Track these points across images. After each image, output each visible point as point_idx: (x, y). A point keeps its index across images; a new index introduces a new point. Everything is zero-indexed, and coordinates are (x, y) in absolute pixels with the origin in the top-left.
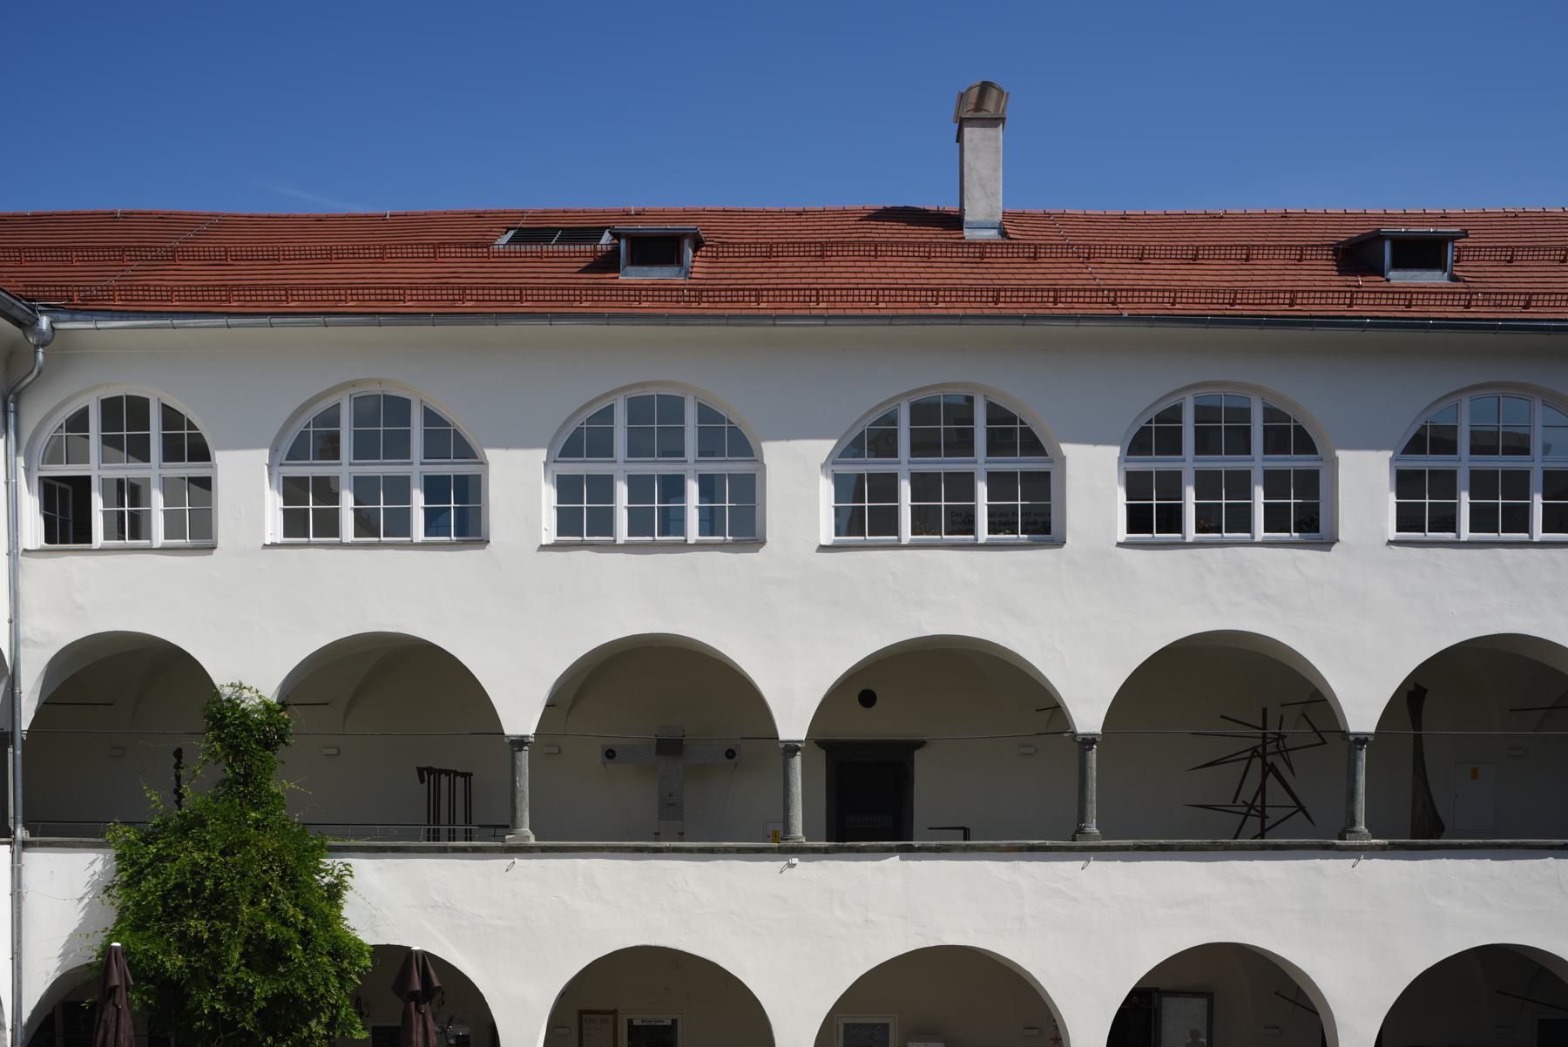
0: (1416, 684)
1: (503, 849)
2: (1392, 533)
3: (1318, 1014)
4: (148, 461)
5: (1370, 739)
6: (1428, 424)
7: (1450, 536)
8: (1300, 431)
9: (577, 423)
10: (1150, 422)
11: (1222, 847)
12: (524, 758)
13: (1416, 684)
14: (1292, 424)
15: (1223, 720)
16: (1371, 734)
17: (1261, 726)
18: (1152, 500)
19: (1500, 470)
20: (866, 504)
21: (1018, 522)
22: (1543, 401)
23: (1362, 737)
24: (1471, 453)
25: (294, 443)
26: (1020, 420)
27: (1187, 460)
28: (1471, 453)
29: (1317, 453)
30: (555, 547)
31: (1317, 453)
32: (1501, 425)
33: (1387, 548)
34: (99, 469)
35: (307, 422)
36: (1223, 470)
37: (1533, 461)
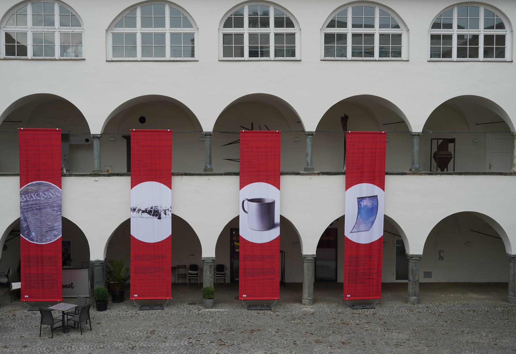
0: (345, 115)
1: (225, 174)
2: (429, 59)
3: (501, 239)
4: (165, 27)
5: (420, 134)
6: (336, 16)
7: (344, 58)
8: (288, 19)
9: (334, 15)
10: (232, 15)
11: (69, 175)
12: (416, 141)
13: (345, 115)
14: (285, 16)
15: (265, 126)
16: (314, 132)
17: (251, 129)
18: (391, 46)
19: (442, 34)
20: (363, 45)
21: (286, 52)
22: (274, 7)
23: (310, 133)
24: (352, 27)
25: (225, 22)
26: (230, 16)
27: (271, 30)
28: (352, 27)
29: (294, 27)
30: (5, 59)
31: (294, 27)
32: (442, 18)
33: (320, 61)
34: (140, 30)
35: (499, 16)
36: (233, 33)
37: (453, 31)
